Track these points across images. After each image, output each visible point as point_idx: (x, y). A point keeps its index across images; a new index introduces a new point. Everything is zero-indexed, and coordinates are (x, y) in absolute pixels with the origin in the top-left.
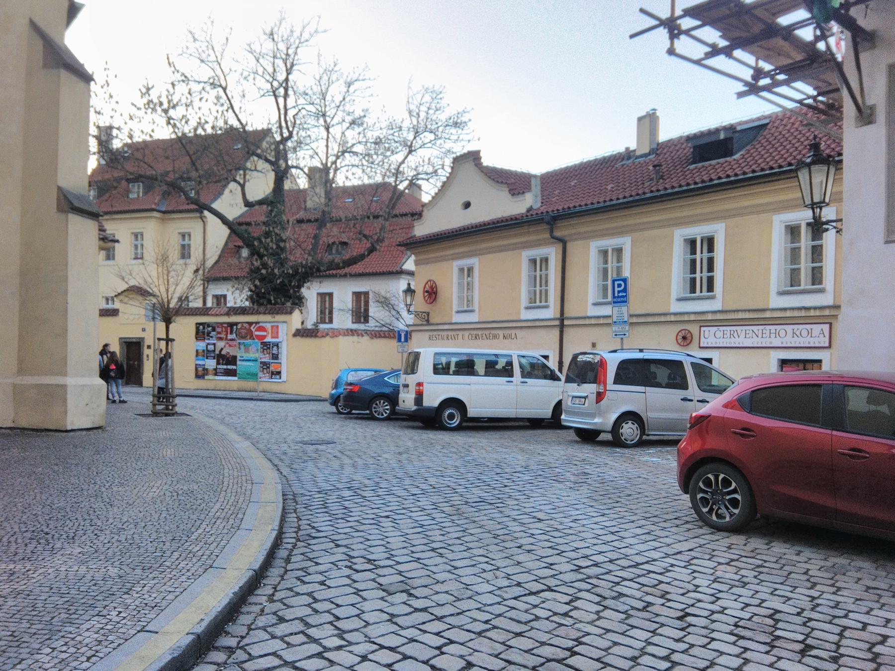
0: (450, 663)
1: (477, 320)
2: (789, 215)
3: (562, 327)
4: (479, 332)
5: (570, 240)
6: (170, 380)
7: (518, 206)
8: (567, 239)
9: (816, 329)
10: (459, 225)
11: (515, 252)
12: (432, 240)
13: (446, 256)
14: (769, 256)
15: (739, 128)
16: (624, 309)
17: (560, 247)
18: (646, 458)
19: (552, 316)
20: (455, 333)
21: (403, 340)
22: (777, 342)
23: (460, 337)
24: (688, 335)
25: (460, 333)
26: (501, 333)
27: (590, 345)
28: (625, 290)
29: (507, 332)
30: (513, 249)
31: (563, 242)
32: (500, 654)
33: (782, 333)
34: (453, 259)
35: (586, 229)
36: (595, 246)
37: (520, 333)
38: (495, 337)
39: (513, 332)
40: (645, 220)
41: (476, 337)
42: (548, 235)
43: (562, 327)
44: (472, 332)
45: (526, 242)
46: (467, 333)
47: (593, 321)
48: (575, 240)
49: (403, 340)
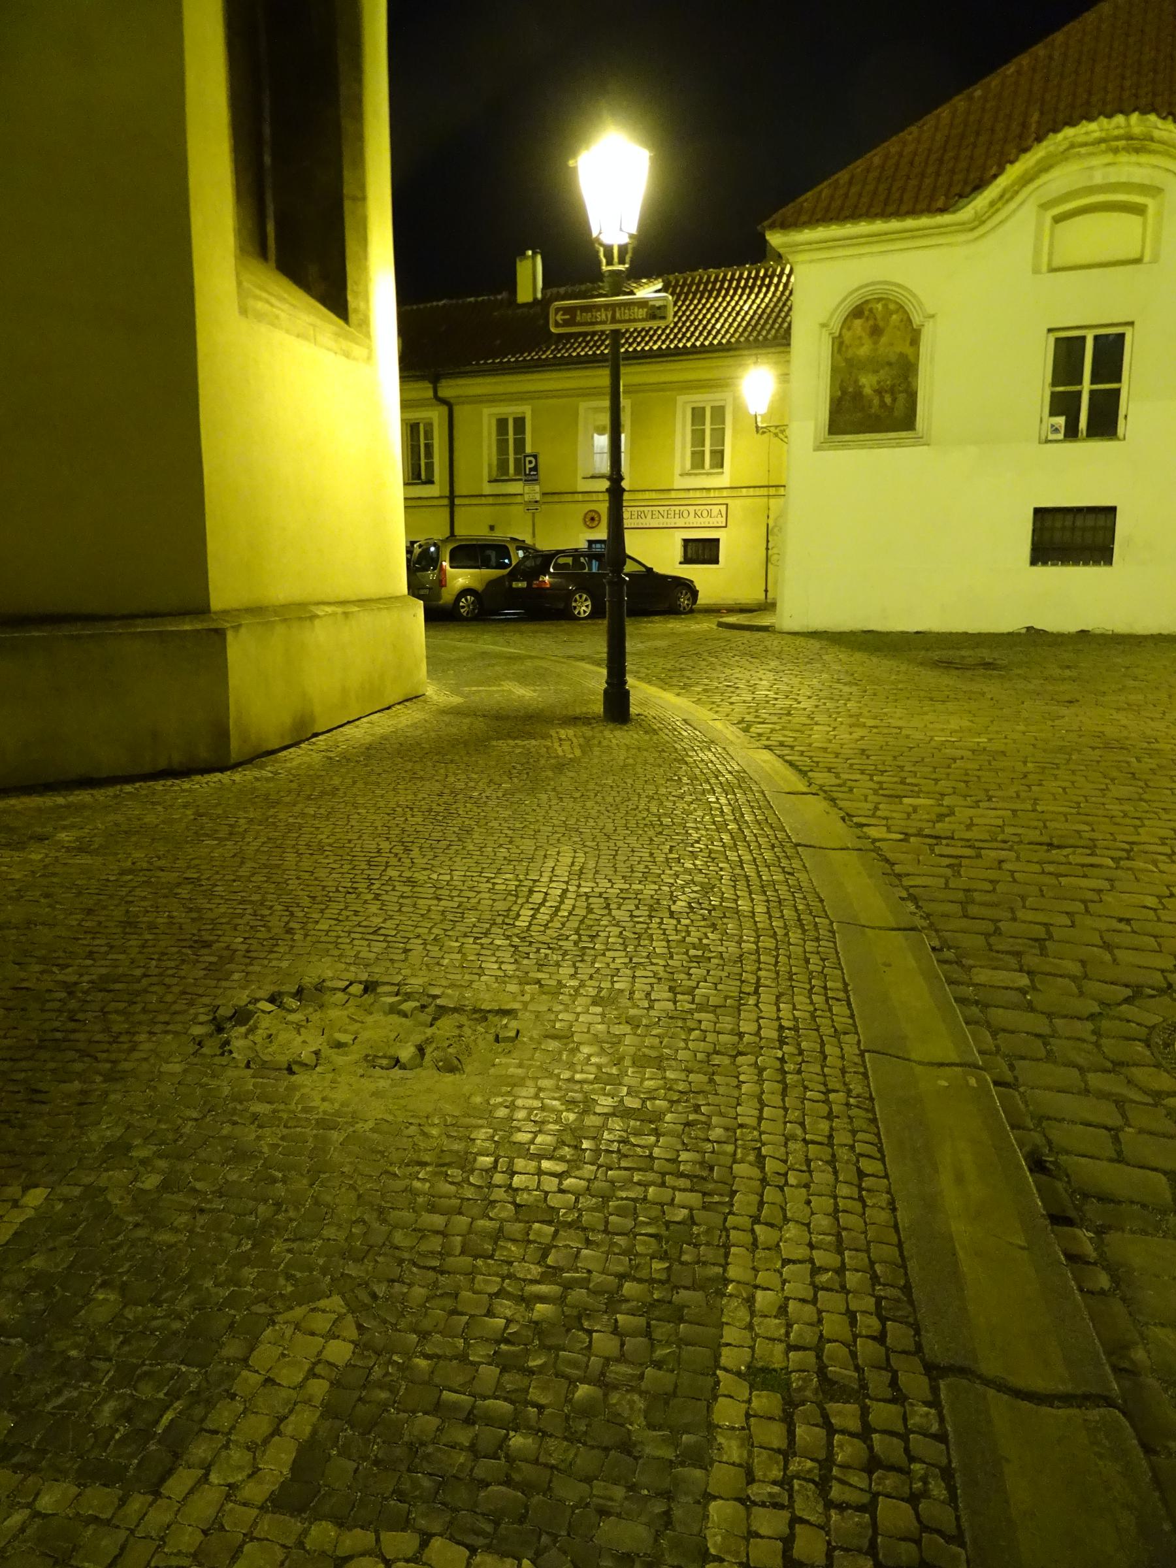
0: (766, 1552)
3: (452, 506)
5: (458, 404)
8: (452, 401)
9: (715, 509)
14: (1107, 336)
15: (651, 303)
16: (537, 488)
17: (445, 409)
19: (437, 494)
22: (681, 523)
24: (589, 517)
27: (488, 529)
28: (535, 468)
31: (448, 404)
32: (934, 1437)
33: (685, 514)
36: (488, 416)
42: (430, 394)
43: (452, 506)
48: (463, 403)
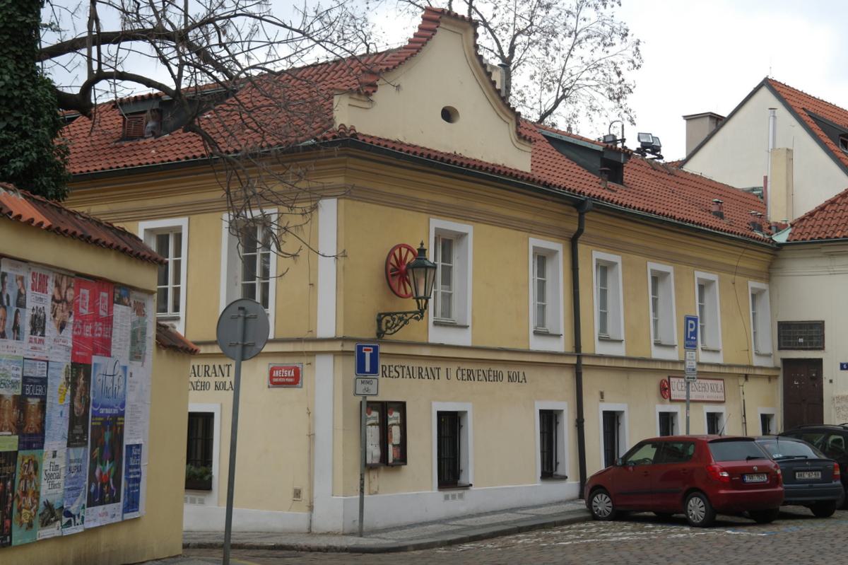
1: (469, 344)
2: (664, 266)
3: (578, 370)
4: (474, 367)
6: (439, 539)
7: (520, 161)
10: (478, 157)
11: (521, 234)
12: (432, 165)
13: (418, 201)
18: (729, 532)
20: (433, 365)
21: (368, 369)
23: (443, 373)
25: (443, 367)
26: (505, 371)
29: (513, 370)
30: (518, 229)
34: (531, 231)
35: (386, 189)
37: (530, 373)
38: (498, 377)
39: (521, 370)
40: (681, 251)
41: (470, 376)
44: (466, 366)
45: (521, 221)
46: (454, 367)
47: (607, 363)
49: (368, 369)
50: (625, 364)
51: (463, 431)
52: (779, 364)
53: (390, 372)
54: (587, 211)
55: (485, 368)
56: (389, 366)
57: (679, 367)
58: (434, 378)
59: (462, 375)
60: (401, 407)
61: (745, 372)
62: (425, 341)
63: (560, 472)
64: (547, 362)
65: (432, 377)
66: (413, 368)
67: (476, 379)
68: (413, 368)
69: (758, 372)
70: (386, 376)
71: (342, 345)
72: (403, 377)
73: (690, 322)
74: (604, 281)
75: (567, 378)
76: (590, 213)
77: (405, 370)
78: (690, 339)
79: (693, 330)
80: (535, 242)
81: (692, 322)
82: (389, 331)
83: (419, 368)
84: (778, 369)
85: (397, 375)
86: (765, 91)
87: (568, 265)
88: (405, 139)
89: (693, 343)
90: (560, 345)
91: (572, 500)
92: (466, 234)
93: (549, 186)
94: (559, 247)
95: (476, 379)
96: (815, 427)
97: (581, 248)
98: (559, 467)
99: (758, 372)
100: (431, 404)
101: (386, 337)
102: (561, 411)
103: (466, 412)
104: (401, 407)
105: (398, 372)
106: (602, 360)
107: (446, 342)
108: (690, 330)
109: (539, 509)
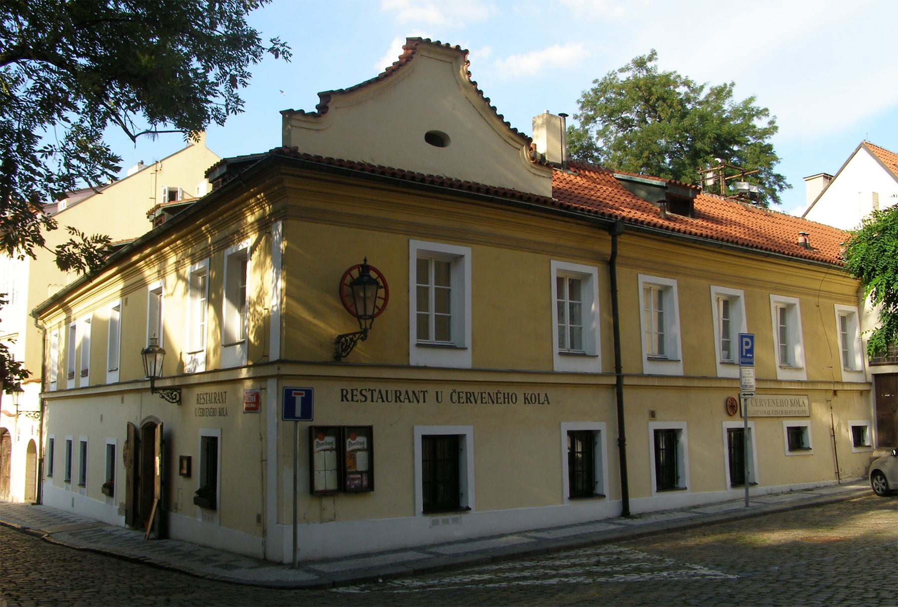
3: (618, 388)
23: (431, 396)
25: (431, 390)
29: (530, 391)
38: (509, 399)
46: (446, 391)
47: (657, 382)
50: (680, 383)
51: (597, 447)
52: (870, 378)
53: (352, 395)
54: (620, 234)
55: (492, 390)
56: (352, 391)
57: (736, 384)
58: (418, 402)
59: (459, 398)
60: (368, 432)
61: (832, 387)
62: (405, 364)
63: (598, 490)
64: (578, 383)
65: (415, 400)
66: (387, 391)
67: (479, 401)
68: (387, 391)
69: (846, 387)
70: (348, 400)
71: (279, 369)
72: (372, 401)
73: (745, 340)
74: (660, 305)
75: (606, 399)
76: (623, 236)
77: (376, 394)
78: (746, 357)
79: (748, 347)
80: (558, 266)
81: (748, 340)
82: (344, 354)
83: (342, 390)
84: (870, 384)
85: (363, 399)
86: (862, 151)
87: (657, 299)
88: (373, 161)
89: (749, 360)
90: (594, 366)
91: (608, 520)
92: (462, 256)
93: (568, 208)
94: (594, 271)
95: (479, 401)
96: (158, 472)
97: (622, 272)
98: (680, 480)
99: (846, 387)
100: (413, 428)
101: (343, 360)
102: (599, 431)
103: (465, 435)
104: (368, 432)
105: (365, 396)
106: (650, 379)
107: (429, 365)
108: (745, 347)
109: (367, 559)
